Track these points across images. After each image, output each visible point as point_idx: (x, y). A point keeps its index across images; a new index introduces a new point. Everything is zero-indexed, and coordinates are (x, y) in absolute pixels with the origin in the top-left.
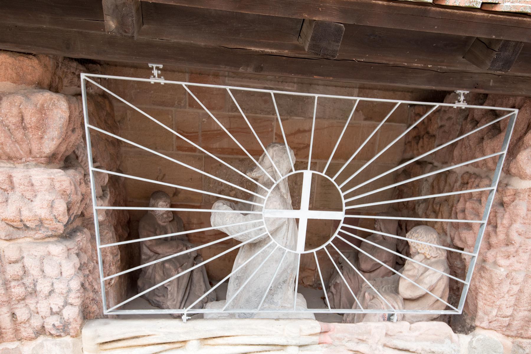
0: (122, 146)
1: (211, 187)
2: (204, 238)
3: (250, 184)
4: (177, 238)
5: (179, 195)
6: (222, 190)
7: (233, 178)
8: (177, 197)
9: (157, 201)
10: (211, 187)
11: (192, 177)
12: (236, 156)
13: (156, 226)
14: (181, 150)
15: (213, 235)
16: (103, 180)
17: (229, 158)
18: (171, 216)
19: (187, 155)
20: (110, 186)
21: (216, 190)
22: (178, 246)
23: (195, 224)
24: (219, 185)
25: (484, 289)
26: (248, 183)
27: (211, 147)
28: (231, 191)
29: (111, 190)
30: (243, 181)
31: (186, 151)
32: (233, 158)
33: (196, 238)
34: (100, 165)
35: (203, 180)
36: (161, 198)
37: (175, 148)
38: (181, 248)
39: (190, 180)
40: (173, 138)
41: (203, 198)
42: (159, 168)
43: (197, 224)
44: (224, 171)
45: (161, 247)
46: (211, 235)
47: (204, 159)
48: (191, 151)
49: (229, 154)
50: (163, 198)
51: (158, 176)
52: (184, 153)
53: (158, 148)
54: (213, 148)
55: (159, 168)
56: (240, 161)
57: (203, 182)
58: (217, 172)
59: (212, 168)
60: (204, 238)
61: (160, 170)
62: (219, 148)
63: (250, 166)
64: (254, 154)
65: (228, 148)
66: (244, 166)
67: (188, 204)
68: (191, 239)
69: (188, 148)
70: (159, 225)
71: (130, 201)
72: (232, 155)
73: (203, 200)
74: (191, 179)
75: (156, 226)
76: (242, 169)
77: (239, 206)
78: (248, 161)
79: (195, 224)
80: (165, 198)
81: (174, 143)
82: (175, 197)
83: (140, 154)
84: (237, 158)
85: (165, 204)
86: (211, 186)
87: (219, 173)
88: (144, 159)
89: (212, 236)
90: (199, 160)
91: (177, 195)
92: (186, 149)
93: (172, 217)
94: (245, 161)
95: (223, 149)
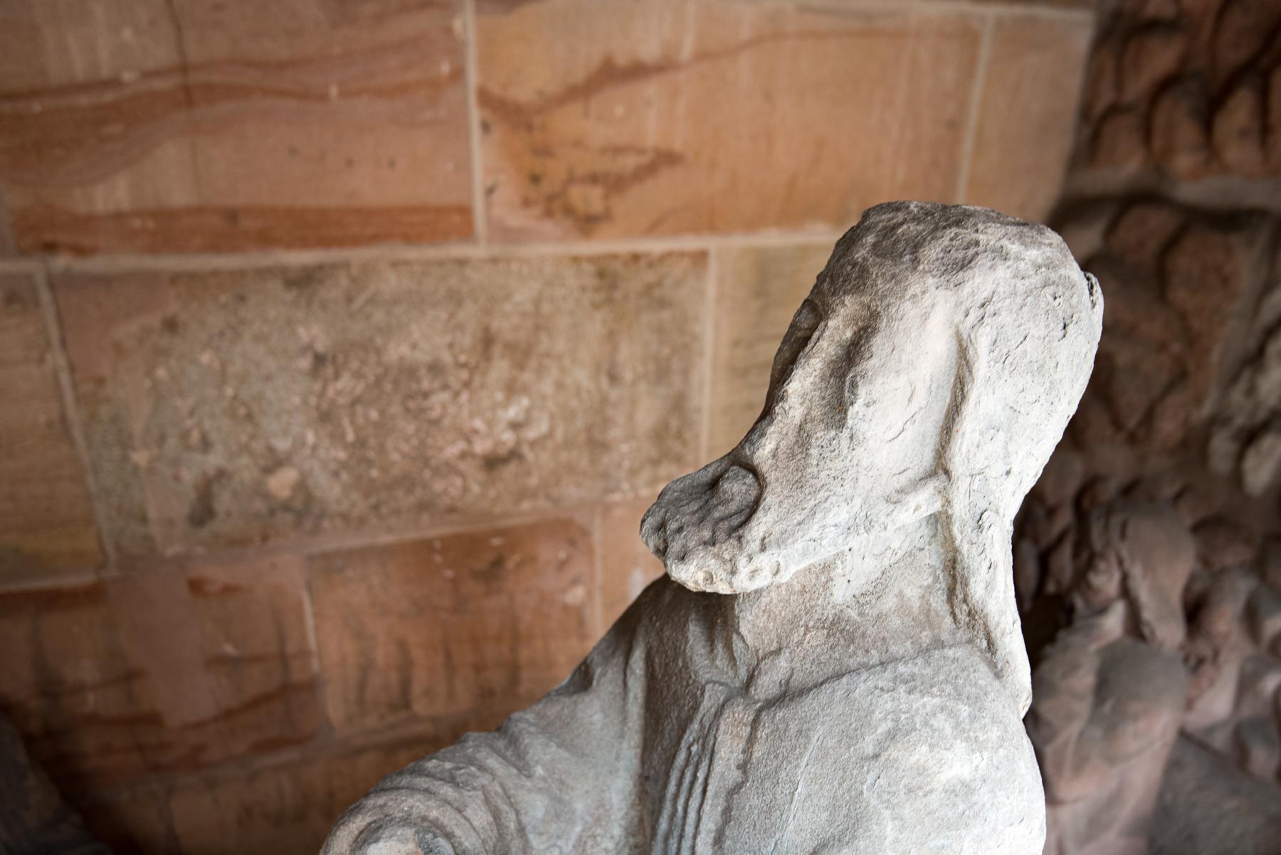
27: (81, 208)
35: (77, 433)
58: (161, 373)
59: (119, 349)
77: (539, 771)
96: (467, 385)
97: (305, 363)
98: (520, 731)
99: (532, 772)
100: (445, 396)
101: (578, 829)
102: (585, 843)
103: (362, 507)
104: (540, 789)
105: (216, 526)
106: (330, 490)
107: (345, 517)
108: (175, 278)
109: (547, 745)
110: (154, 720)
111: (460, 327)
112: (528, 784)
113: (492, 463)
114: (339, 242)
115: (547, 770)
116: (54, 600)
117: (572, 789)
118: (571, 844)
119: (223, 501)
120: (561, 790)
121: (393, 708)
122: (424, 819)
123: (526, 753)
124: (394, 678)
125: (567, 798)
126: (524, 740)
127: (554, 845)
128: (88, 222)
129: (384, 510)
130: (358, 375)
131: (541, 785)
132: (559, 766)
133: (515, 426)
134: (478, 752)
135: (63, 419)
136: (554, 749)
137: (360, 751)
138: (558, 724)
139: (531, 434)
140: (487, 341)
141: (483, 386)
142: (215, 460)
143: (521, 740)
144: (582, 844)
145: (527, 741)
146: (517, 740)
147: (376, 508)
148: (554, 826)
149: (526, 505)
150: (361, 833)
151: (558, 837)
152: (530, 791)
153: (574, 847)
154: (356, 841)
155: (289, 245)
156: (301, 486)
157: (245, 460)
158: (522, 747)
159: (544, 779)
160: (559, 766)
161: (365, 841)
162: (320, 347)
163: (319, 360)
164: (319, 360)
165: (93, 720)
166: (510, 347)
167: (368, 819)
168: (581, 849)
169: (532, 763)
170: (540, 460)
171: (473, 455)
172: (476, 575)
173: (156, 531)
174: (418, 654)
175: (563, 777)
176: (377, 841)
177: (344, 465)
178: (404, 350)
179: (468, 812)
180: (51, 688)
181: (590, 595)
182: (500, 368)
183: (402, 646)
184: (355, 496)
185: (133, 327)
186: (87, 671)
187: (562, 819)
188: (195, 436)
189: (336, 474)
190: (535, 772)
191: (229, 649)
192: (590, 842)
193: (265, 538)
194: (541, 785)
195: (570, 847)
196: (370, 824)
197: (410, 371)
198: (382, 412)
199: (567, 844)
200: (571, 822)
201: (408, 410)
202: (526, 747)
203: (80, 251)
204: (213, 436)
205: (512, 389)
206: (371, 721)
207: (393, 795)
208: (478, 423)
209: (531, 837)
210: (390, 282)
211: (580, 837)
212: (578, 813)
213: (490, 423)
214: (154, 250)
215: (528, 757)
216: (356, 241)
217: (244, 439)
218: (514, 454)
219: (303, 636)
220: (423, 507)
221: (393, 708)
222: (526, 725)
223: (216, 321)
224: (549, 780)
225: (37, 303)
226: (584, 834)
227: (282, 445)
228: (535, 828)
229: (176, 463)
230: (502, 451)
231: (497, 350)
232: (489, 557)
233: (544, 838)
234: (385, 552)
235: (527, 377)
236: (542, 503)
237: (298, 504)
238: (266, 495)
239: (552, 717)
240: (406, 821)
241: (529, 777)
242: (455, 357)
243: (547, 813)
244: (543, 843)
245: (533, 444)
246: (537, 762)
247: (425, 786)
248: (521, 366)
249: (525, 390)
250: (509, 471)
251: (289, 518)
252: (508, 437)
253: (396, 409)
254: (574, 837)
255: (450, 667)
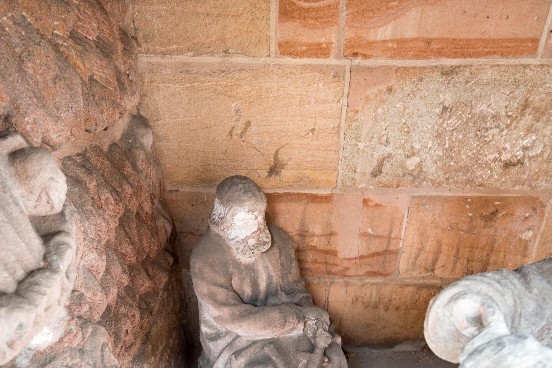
0: (140, 52)
1: (362, 148)
2: (335, 265)
3: (461, 137)
4: (281, 287)
5: (284, 172)
6: (386, 155)
7: (419, 124)
8: (278, 177)
9: (231, 211)
10: (362, 148)
11: (315, 124)
12: (433, 62)
13: (231, 269)
14: (290, 54)
15: (356, 258)
16: (44, 198)
17: (414, 68)
18: (266, 240)
19: (304, 66)
20: (97, 186)
21: (372, 156)
22: (286, 322)
23: (318, 236)
24: (380, 143)
25: (532, 163)
26: (455, 134)
27: (371, 39)
28: (408, 157)
29: (103, 197)
30: (445, 129)
31: (301, 55)
32: (425, 68)
33: (317, 265)
34: (25, 145)
35: (342, 133)
36: (240, 202)
37: (274, 48)
38: (291, 326)
39: (311, 134)
40: (269, 19)
41: (339, 178)
42: (233, 105)
43: (322, 235)
44: (398, 106)
45: (245, 325)
46: (350, 259)
47: (348, 75)
48: (316, 55)
49: (417, 57)
50: (247, 203)
51: (233, 127)
52: (299, 61)
53: (230, 51)
54: (374, 42)
55: (233, 105)
56: (443, 74)
57: (342, 136)
58: (380, 110)
59: (367, 99)
60: (335, 265)
61: (237, 111)
62: (392, 41)
63: (470, 87)
64: (488, 50)
65: (416, 39)
66: (452, 89)
67: (302, 192)
68: (306, 267)
69: (310, 45)
70: (237, 264)
71: (171, 192)
72: (425, 57)
73: (339, 182)
74: (313, 130)
75: (231, 269)
76: (447, 96)
77: (535, 291)
78: (467, 74)
79: (318, 236)
80: (253, 202)
81: (272, 34)
82: (273, 176)
83: (188, 72)
84: (436, 67)
85: (254, 217)
86: (361, 145)
87: (384, 113)
88: (196, 84)
89: (354, 261)
90: (336, 79)
91: (277, 173)
92: (304, 48)
93: (268, 243)
94: (457, 74)
95: (401, 42)
96: (508, 126)
97: (438, 110)
98: (529, 272)
99: (531, 291)
100: (496, 131)
101: (544, 323)
102: (544, 331)
103: (442, 177)
104: (534, 299)
105: (380, 178)
106: (431, 169)
107: (433, 181)
108: (397, 69)
109: (542, 281)
110: (334, 253)
111: (514, 98)
112: (529, 295)
113: (507, 165)
114: (471, 56)
115: (539, 292)
116: (315, 198)
117: (548, 304)
118: (538, 329)
119: (387, 168)
120: (543, 302)
121: (427, 270)
122: (486, 295)
123: (530, 282)
124: (431, 257)
125: (544, 307)
126: (530, 276)
127: (530, 327)
128: (372, 44)
129: (451, 181)
130: (459, 118)
131: (535, 297)
132: (545, 291)
133: (525, 149)
134: (509, 275)
135: (339, 126)
136: (545, 283)
137: (407, 285)
138: (548, 273)
139: (531, 153)
140: (525, 105)
141: (516, 127)
142: (389, 150)
143: (529, 276)
144: (542, 331)
145: (531, 277)
146: (526, 275)
147: (447, 179)
148: (534, 318)
149: (517, 188)
150: (455, 295)
151: (534, 324)
152: (529, 298)
153: (538, 331)
154: (452, 297)
155: (448, 57)
156: (419, 166)
157: (400, 151)
158: (528, 279)
159: (537, 295)
160: (545, 291)
161: (457, 298)
162: (447, 104)
163: (445, 109)
164: (445, 109)
165: (314, 248)
166: (536, 109)
167: (460, 290)
168: (541, 333)
169: (532, 287)
170: (532, 167)
171: (500, 160)
172: (482, 217)
173: (358, 176)
174: (444, 248)
175: (546, 297)
176: (464, 298)
177: (440, 158)
178: (484, 107)
179: (506, 297)
180: (304, 233)
181: (535, 236)
182: (528, 119)
183: (439, 243)
184: (441, 173)
185: (375, 90)
186: (316, 229)
187: (538, 316)
188: (385, 138)
189: (436, 162)
190: (533, 291)
191: (370, 231)
192: (546, 332)
193: (398, 186)
194: (535, 297)
195: (537, 331)
196: (460, 292)
197: (483, 118)
198: (464, 136)
199: (536, 329)
200: (542, 319)
201: (476, 136)
202: (530, 279)
203: (365, 56)
204: (391, 139)
205: (529, 130)
206: (415, 274)
207: (474, 282)
208: (507, 146)
209: (522, 320)
210: (489, 74)
211: (543, 327)
212: (546, 316)
213: (513, 146)
214: (392, 57)
215: (531, 284)
216: (479, 55)
217: (403, 142)
218: (520, 162)
219: (400, 231)
220: (468, 182)
221: (427, 270)
222: (532, 270)
223: (407, 89)
224: (539, 296)
225: (344, 78)
226: (546, 326)
227: (417, 146)
228: (525, 316)
229: (373, 149)
230: (515, 160)
231: (528, 110)
232: (493, 209)
233: (527, 322)
234: (446, 200)
235: (539, 125)
236: (526, 187)
237: (415, 174)
238: (403, 167)
239: (546, 269)
240: (478, 293)
241: (530, 292)
242: (507, 113)
243: (533, 311)
244: (526, 324)
245: (530, 158)
246: (535, 287)
247: (488, 282)
248: (538, 120)
249: (536, 131)
250: (514, 170)
251: (410, 178)
252: (520, 154)
253: (471, 135)
254: (540, 326)
255: (457, 257)
